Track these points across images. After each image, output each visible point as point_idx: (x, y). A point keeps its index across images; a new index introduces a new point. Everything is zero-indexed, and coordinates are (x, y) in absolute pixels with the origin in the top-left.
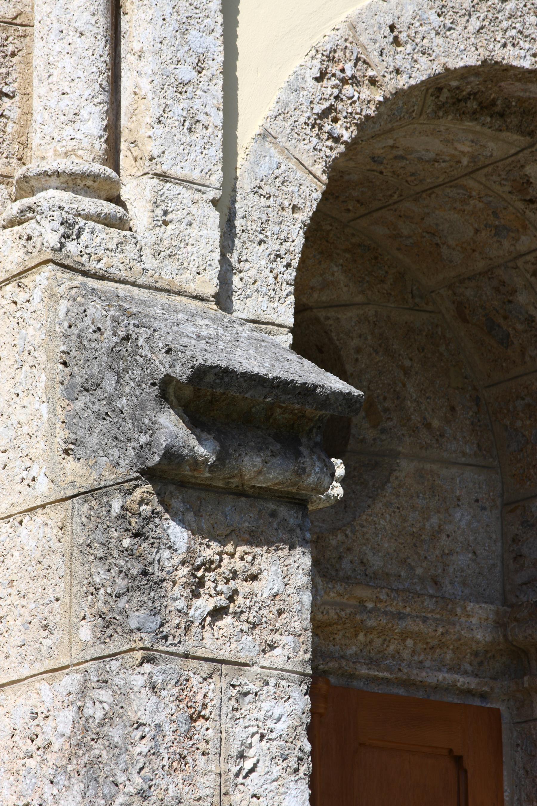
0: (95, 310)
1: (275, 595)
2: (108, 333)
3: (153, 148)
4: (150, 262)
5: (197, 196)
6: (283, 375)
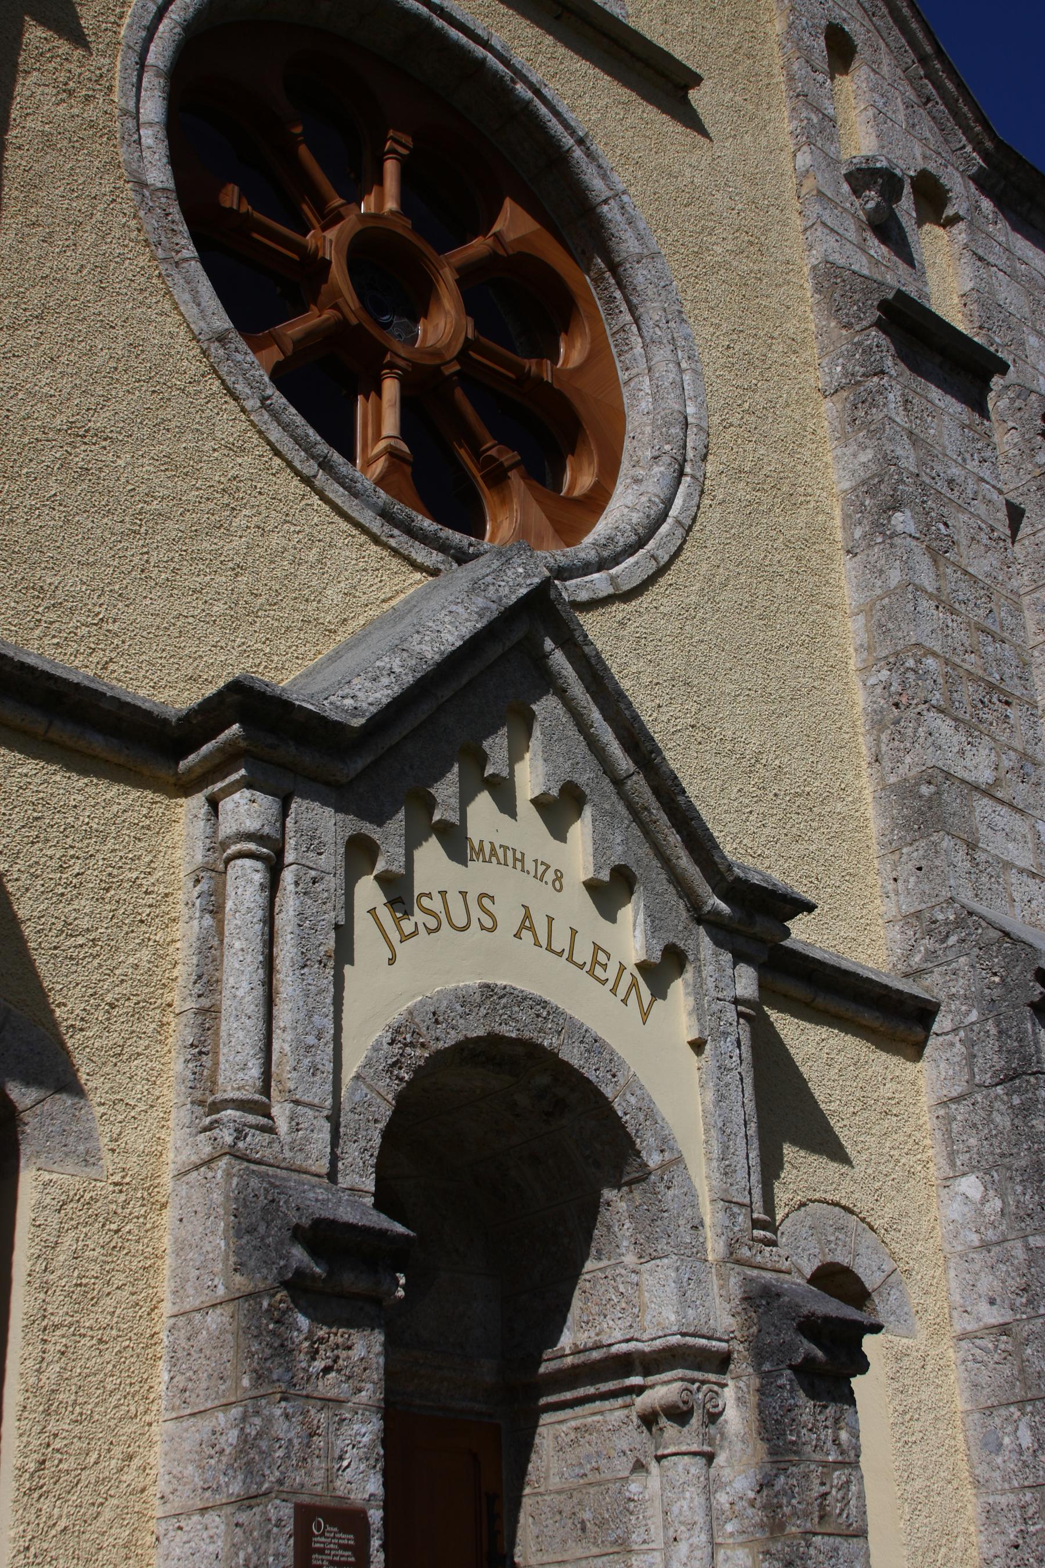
0: (254, 1182)
1: (362, 1359)
2: (262, 1198)
3: (291, 1085)
4: (288, 1154)
5: (317, 1114)
6: (368, 1224)
